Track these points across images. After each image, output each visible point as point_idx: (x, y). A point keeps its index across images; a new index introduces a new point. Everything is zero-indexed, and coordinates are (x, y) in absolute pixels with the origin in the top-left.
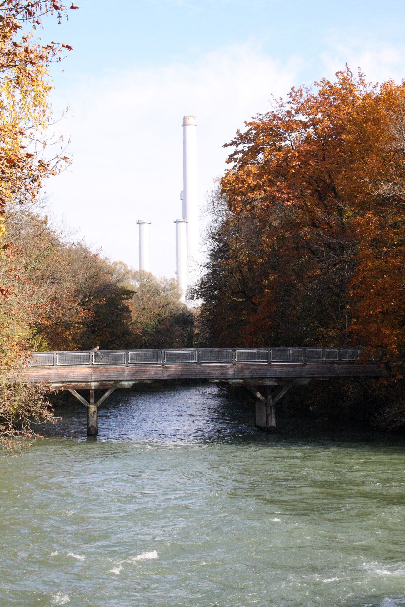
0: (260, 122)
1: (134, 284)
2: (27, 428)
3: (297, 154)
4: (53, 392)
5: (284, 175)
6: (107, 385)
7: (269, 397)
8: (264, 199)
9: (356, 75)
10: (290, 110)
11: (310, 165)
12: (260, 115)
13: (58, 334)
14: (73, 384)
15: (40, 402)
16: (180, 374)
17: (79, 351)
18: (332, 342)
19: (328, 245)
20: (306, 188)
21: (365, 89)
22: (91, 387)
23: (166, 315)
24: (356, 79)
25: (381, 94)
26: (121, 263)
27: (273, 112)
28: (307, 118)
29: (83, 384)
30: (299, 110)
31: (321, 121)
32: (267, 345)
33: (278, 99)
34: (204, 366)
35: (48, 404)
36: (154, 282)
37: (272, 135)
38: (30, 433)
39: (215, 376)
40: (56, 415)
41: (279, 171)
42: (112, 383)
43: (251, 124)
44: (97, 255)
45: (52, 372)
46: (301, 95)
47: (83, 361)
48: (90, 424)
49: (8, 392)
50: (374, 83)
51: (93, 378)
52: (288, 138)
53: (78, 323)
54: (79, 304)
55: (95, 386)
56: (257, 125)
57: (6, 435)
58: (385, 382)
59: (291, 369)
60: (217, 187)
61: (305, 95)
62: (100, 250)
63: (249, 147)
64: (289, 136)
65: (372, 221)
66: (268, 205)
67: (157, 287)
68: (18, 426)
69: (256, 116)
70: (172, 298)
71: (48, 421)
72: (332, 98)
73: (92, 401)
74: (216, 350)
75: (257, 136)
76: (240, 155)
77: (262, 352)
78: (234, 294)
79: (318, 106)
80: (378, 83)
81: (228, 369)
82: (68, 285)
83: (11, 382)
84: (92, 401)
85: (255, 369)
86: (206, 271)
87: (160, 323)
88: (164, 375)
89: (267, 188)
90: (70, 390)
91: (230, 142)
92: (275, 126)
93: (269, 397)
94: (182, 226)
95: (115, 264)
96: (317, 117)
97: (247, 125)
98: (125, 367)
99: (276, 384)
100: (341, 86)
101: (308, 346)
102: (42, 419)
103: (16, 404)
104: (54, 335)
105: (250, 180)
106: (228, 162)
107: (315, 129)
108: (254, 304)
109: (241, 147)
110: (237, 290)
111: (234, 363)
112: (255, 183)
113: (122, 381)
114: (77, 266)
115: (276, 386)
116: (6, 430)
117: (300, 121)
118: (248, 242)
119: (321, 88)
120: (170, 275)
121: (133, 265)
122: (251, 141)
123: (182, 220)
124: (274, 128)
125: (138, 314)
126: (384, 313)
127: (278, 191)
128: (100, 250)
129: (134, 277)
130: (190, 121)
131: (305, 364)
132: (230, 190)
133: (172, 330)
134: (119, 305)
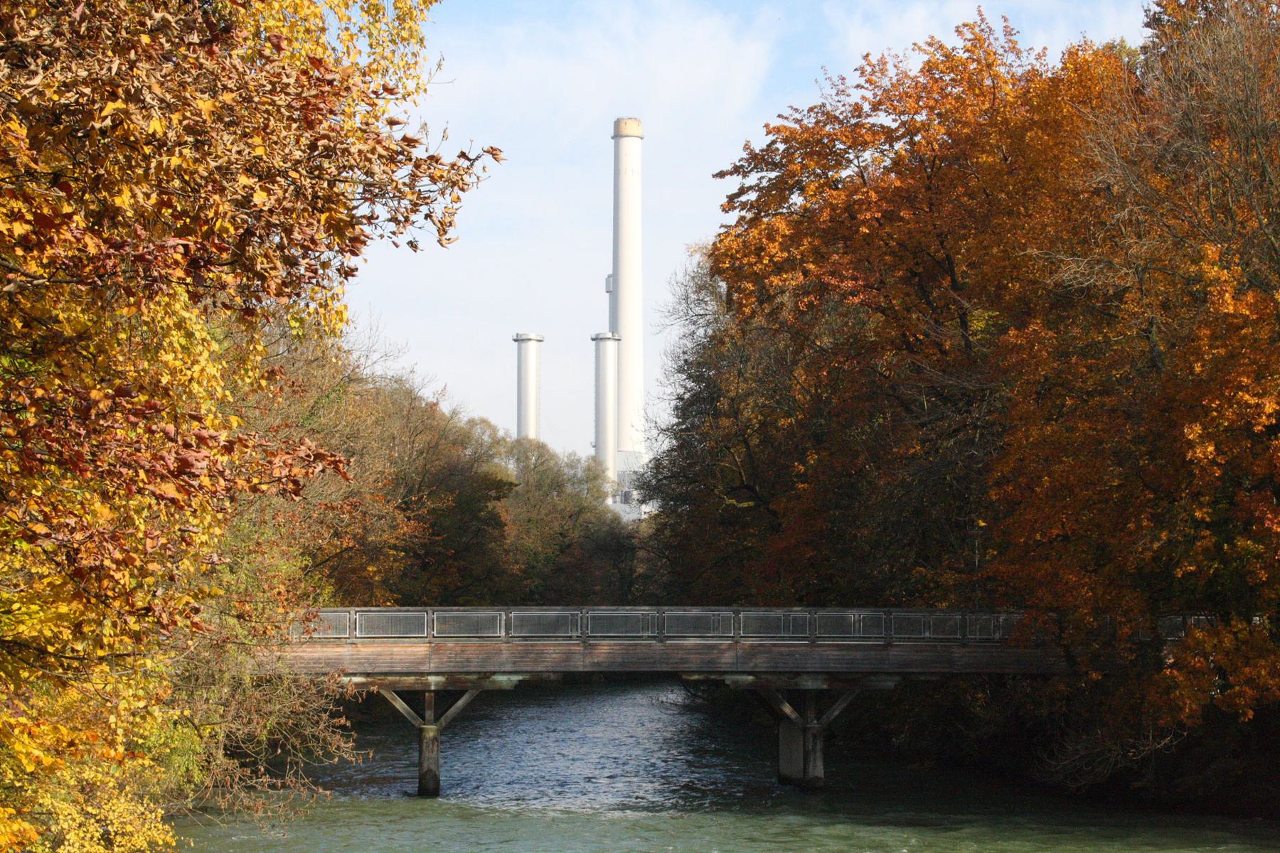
0: (797, 126)
1: (509, 468)
2: (296, 773)
3: (873, 196)
4: (355, 696)
5: (845, 239)
6: (467, 681)
7: (811, 714)
8: (801, 291)
9: (999, 33)
10: (860, 102)
11: (902, 219)
12: (796, 110)
13: (354, 571)
14: (390, 678)
15: (325, 716)
16: (619, 660)
17: (397, 608)
18: (945, 600)
19: (933, 390)
20: (894, 267)
21: (1019, 62)
22: (429, 685)
23: (576, 535)
24: (998, 42)
25: (1063, 69)
26: (484, 421)
27: (824, 105)
28: (894, 120)
29: (411, 679)
30: (880, 103)
31: (925, 127)
32: (800, 601)
33: (835, 79)
34: (671, 645)
35: (343, 721)
36: (552, 463)
37: (819, 154)
38: (303, 785)
39: (694, 667)
40: (359, 746)
41: (834, 231)
42: (474, 677)
43: (778, 130)
44: (436, 405)
45: (344, 651)
46: (883, 71)
47: (409, 629)
48: (425, 765)
49: (257, 694)
50: (1038, 50)
51: (432, 667)
52: (856, 162)
53: (395, 547)
54: (397, 507)
55: (437, 684)
56: (791, 133)
57: (252, 788)
58: (1062, 687)
59: (859, 655)
60: (695, 263)
61: (892, 72)
62: (443, 392)
63: (770, 179)
64: (858, 157)
65: (1040, 340)
66: (811, 303)
67: (559, 473)
68: (277, 768)
69: (787, 112)
70: (590, 499)
71: (341, 758)
72: (947, 78)
73: (429, 714)
74: (695, 612)
75: (788, 153)
76: (752, 196)
77: (795, 618)
78: (732, 492)
79: (919, 92)
80: (1045, 48)
81: (722, 652)
82: (380, 465)
83: (267, 671)
84: (429, 714)
85: (781, 654)
86: (666, 443)
87: (562, 551)
88: (581, 664)
89: (812, 266)
90: (383, 692)
91: (729, 167)
92: (829, 135)
93: (811, 714)
94: (610, 346)
95: (472, 423)
96: (918, 118)
97: (768, 133)
98: (499, 642)
99: (825, 687)
100: (967, 55)
101: (894, 605)
102: (329, 755)
103: (272, 722)
104: (346, 576)
105: (774, 248)
106: (726, 209)
107: (912, 143)
108: (775, 514)
109: (752, 179)
110: (737, 483)
111: (731, 640)
112: (786, 255)
113: (494, 673)
114: (395, 427)
115: (822, 691)
116: (251, 778)
117: (882, 126)
118: (760, 381)
119: (926, 58)
120: (585, 452)
121: (506, 426)
122: (775, 166)
123: (610, 335)
124: (826, 141)
125: (520, 533)
126: (1066, 538)
127: (832, 274)
128: (443, 392)
129: (510, 453)
130: (629, 128)
131: (888, 645)
132: (729, 268)
133: (592, 566)
134: (480, 510)
